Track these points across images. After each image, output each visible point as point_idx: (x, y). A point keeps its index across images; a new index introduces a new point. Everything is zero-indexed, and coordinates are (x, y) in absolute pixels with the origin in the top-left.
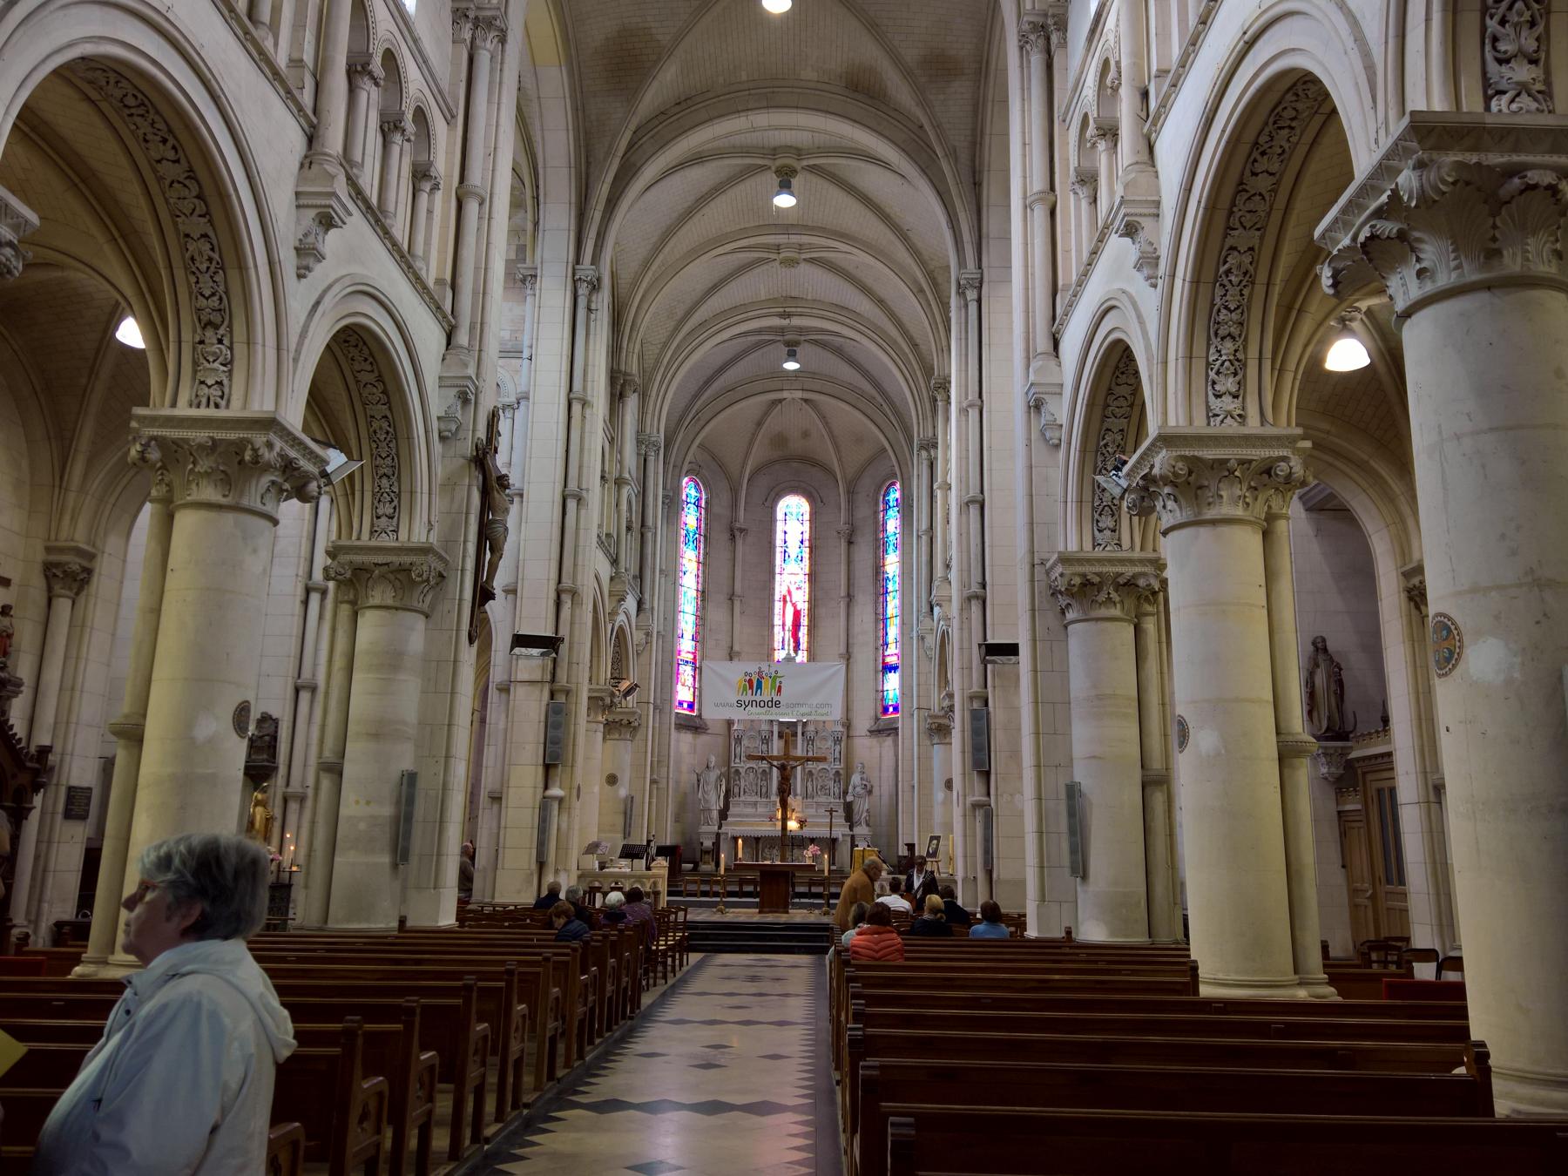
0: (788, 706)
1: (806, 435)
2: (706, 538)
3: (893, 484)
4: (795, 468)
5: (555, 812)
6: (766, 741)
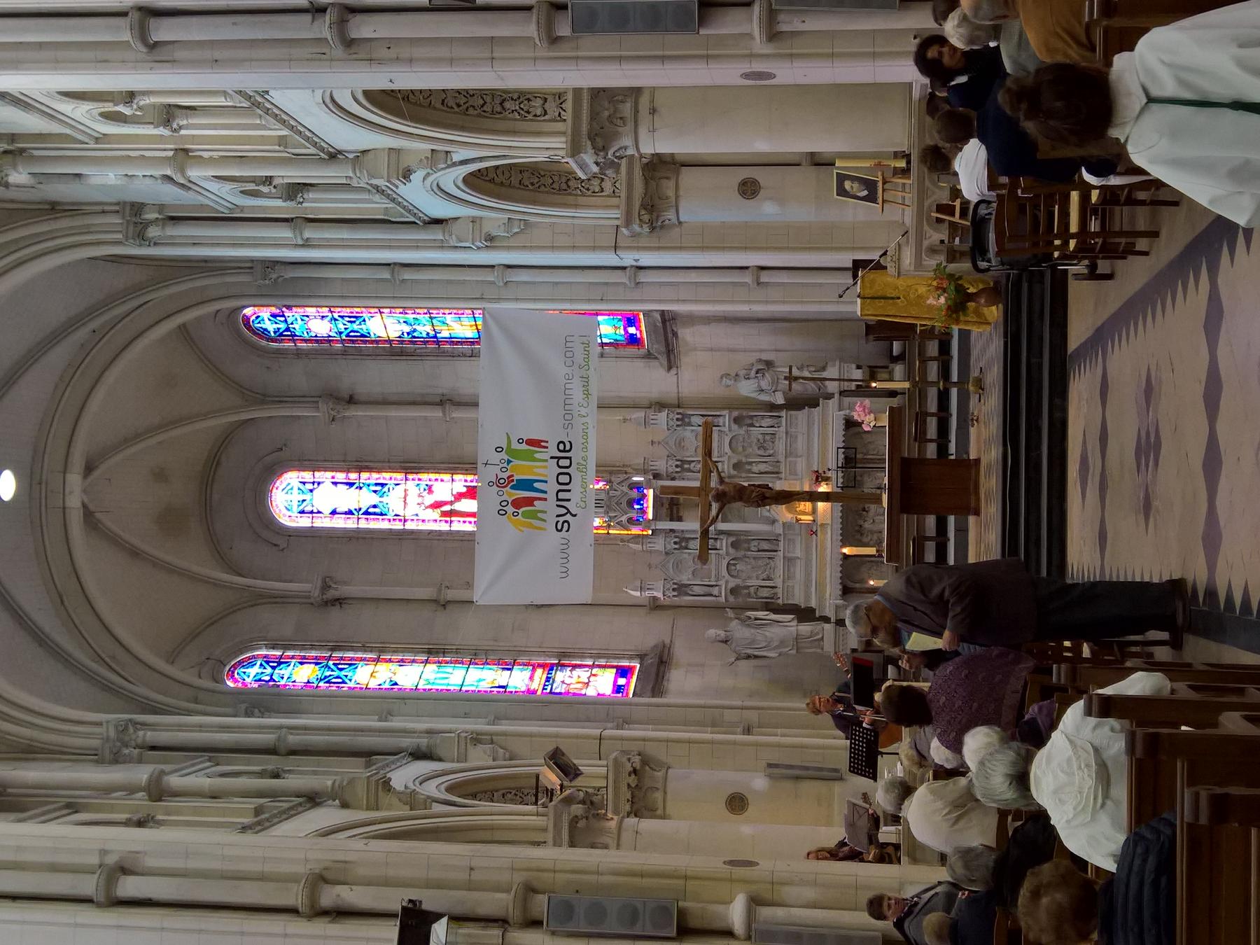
0: (568, 425)
1: (160, 475)
2: (337, 648)
3: (246, 319)
4: (223, 494)
5: (780, 913)
6: (683, 541)
